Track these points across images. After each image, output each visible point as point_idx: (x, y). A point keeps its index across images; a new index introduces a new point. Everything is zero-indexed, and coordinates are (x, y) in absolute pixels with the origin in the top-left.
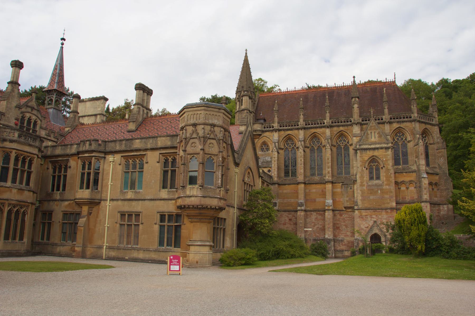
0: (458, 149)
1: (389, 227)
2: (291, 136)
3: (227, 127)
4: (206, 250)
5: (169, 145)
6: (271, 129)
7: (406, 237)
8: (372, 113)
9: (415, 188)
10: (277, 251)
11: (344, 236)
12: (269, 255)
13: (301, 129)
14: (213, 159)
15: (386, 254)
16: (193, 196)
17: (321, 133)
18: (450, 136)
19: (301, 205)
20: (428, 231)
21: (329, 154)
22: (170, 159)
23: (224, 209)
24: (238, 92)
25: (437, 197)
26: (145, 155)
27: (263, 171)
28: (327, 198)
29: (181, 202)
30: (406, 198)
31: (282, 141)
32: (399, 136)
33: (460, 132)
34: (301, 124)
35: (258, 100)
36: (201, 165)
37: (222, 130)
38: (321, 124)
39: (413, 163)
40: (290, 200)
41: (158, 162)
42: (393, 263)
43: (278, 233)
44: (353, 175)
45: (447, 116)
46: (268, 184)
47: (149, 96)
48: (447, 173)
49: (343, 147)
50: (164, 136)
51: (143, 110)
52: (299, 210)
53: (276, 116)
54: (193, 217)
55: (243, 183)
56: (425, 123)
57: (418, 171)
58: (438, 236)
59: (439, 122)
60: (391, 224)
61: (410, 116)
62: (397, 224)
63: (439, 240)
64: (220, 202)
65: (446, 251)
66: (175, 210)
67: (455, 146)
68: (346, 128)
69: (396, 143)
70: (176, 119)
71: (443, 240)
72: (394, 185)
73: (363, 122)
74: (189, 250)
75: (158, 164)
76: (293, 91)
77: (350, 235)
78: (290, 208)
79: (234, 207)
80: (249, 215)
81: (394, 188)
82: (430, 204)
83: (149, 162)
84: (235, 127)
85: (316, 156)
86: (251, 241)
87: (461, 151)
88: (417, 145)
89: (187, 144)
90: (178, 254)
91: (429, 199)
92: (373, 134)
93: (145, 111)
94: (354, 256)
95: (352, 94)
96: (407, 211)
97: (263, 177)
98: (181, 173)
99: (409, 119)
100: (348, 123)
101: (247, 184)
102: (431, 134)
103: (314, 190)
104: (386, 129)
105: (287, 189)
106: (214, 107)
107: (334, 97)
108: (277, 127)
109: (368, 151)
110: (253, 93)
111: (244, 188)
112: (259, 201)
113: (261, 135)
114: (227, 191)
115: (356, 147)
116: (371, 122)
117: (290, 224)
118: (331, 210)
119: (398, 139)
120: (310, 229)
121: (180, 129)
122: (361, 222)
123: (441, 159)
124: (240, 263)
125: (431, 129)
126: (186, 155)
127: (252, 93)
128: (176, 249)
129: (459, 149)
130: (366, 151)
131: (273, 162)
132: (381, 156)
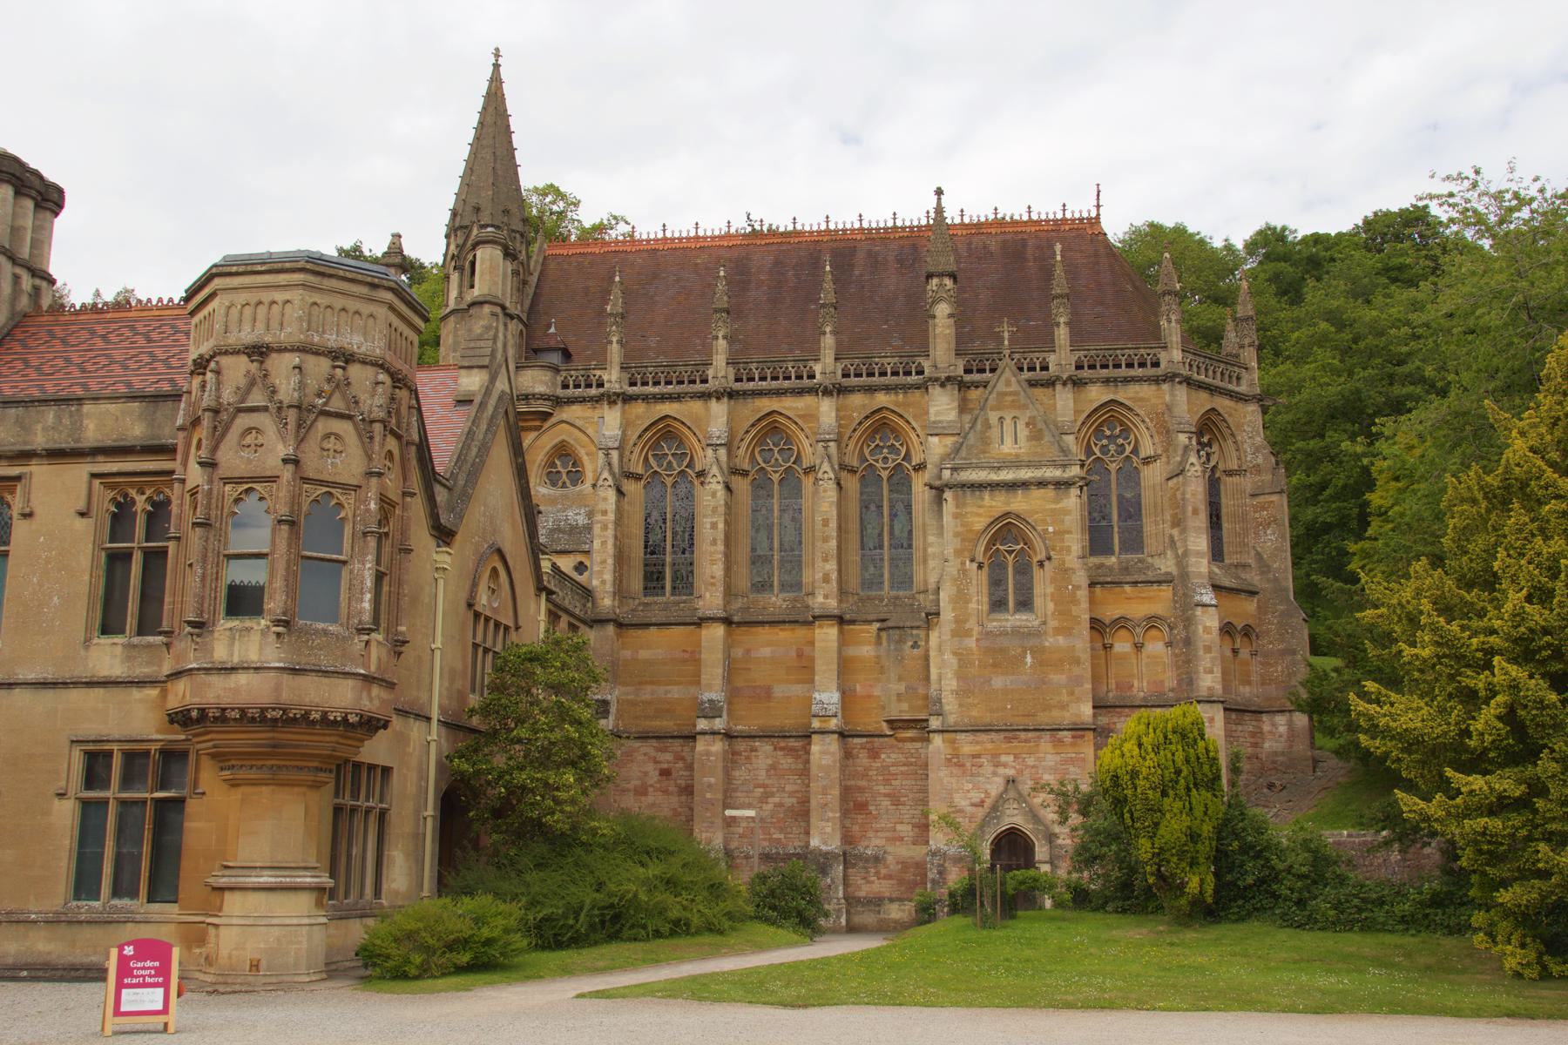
0: (1320, 498)
1: (1068, 804)
4: (299, 908)
5: (135, 438)
6: (593, 391)
7: (1142, 841)
8: (1006, 342)
9: (1169, 644)
10: (612, 906)
11: (888, 839)
12: (578, 926)
13: (718, 395)
14: (340, 505)
15: (1059, 912)
16: (244, 668)
17: (799, 416)
19: (712, 711)
20: (1227, 819)
22: (141, 503)
23: (385, 726)
24: (457, 228)
25: (1249, 683)
26: (18, 478)
27: (555, 568)
28: (817, 683)
29: (188, 694)
34: (720, 375)
35: (539, 269)
36: (285, 527)
37: (382, 377)
40: (667, 692)
41: (82, 514)
42: (1092, 950)
43: (618, 828)
44: (925, 591)
45: (1281, 368)
47: (48, 214)
49: (885, 474)
50: (114, 398)
51: (16, 278)
52: (703, 733)
53: (615, 339)
54: (240, 763)
55: (471, 616)
57: (1179, 581)
58: (1265, 837)
60: (1077, 788)
61: (1154, 359)
62: (1106, 791)
64: (365, 694)
65: (1295, 895)
66: (158, 732)
67: (1311, 485)
69: (1095, 465)
71: (1281, 853)
72: (1086, 632)
73: (968, 378)
75: (81, 524)
77: (911, 834)
78: (665, 723)
79: (429, 719)
80: (491, 753)
81: (1089, 645)
83: (38, 510)
85: (776, 507)
86: (499, 866)
87: (1334, 506)
88: (1177, 475)
89: (223, 435)
90: (163, 933)
91: (1220, 692)
92: (1008, 422)
93: (27, 282)
94: (929, 922)
95: (928, 259)
96: (1147, 734)
97: (552, 593)
98: (191, 565)
99: (1150, 371)
100: (909, 378)
101: (487, 619)
102: (1233, 435)
103: (766, 652)
104: (1058, 407)
105: (656, 646)
106: (349, 275)
107: (857, 273)
108: (617, 386)
109: (987, 495)
110: (522, 235)
112: (534, 691)
114: (398, 645)
115: (940, 478)
116: (1003, 378)
117: (666, 792)
118: (833, 732)
119: (1104, 450)
120: (751, 813)
121: (190, 366)
122: (953, 780)
123: (1269, 532)
124: (449, 964)
125: (1230, 415)
126: (217, 485)
127: (518, 236)
128: (156, 907)
129: (1326, 501)
131: (597, 529)
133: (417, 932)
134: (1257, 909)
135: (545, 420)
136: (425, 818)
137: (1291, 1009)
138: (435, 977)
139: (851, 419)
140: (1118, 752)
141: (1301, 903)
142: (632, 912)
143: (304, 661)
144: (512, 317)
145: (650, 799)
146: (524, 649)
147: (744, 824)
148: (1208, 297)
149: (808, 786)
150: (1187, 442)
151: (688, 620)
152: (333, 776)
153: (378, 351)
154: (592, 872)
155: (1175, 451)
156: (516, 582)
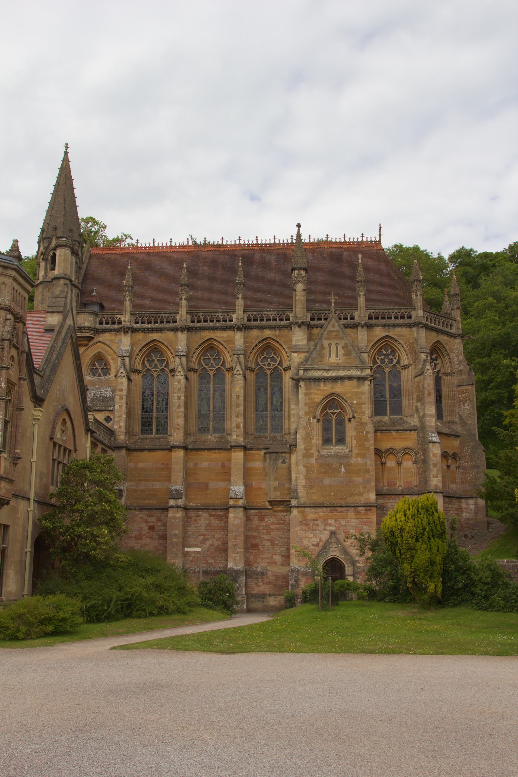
1: (365, 545)
2: (160, 344)
3: (21, 312)
6: (116, 326)
7: (405, 565)
8: (333, 305)
9: (415, 462)
10: (127, 599)
11: (268, 563)
12: (110, 610)
13: (182, 330)
15: (361, 602)
17: (225, 341)
18: (475, 362)
19: (177, 495)
21: (241, 387)
23: (8, 503)
24: (44, 238)
25: (455, 483)
28: (232, 481)
30: (396, 484)
31: (138, 354)
32: (386, 355)
33: (494, 354)
34: (183, 319)
35: (87, 261)
37: (9, 316)
38: (225, 321)
42: (380, 622)
43: (130, 558)
44: (289, 434)
46: (106, 448)
48: (475, 435)
49: (269, 372)
52: (172, 507)
53: (128, 299)
55: (51, 444)
58: (468, 563)
59: (462, 330)
60: (369, 537)
62: (387, 539)
63: (469, 572)
65: (483, 593)
67: (484, 380)
68: (278, 332)
69: (378, 370)
72: (372, 456)
73: (312, 323)
76: (166, 247)
77: (280, 560)
78: (152, 501)
79: (29, 499)
80: (62, 517)
81: (374, 463)
82: (444, 496)
85: (211, 389)
87: (496, 391)
88: (420, 375)
92: (333, 346)
94: (291, 607)
95: (293, 261)
96: (409, 509)
99: (406, 321)
100: (282, 322)
101: (60, 446)
102: (448, 355)
103: (206, 464)
104: (359, 338)
107: (255, 267)
108: (129, 324)
109: (322, 384)
110: (79, 243)
111: (53, 456)
113: (93, 338)
114: (15, 460)
115: (298, 374)
116: (331, 323)
117: (152, 538)
119: (382, 361)
120: (199, 550)
123: (466, 405)
125: (447, 344)
127: (77, 243)
129: (491, 389)
130: (317, 383)
131: (117, 399)
132: (347, 395)
133: (24, 614)
134: (464, 601)
135: (90, 341)
136: (26, 552)
137: (486, 653)
138: (34, 639)
139: (251, 343)
140: (394, 519)
141: (486, 597)
142: (138, 603)
144: (75, 286)
145: (143, 542)
146: (81, 462)
147: (193, 555)
148: (431, 284)
149: (227, 535)
150: (425, 357)
151: (165, 447)
153: (7, 302)
154: (116, 581)
155: (419, 362)
156: (75, 426)
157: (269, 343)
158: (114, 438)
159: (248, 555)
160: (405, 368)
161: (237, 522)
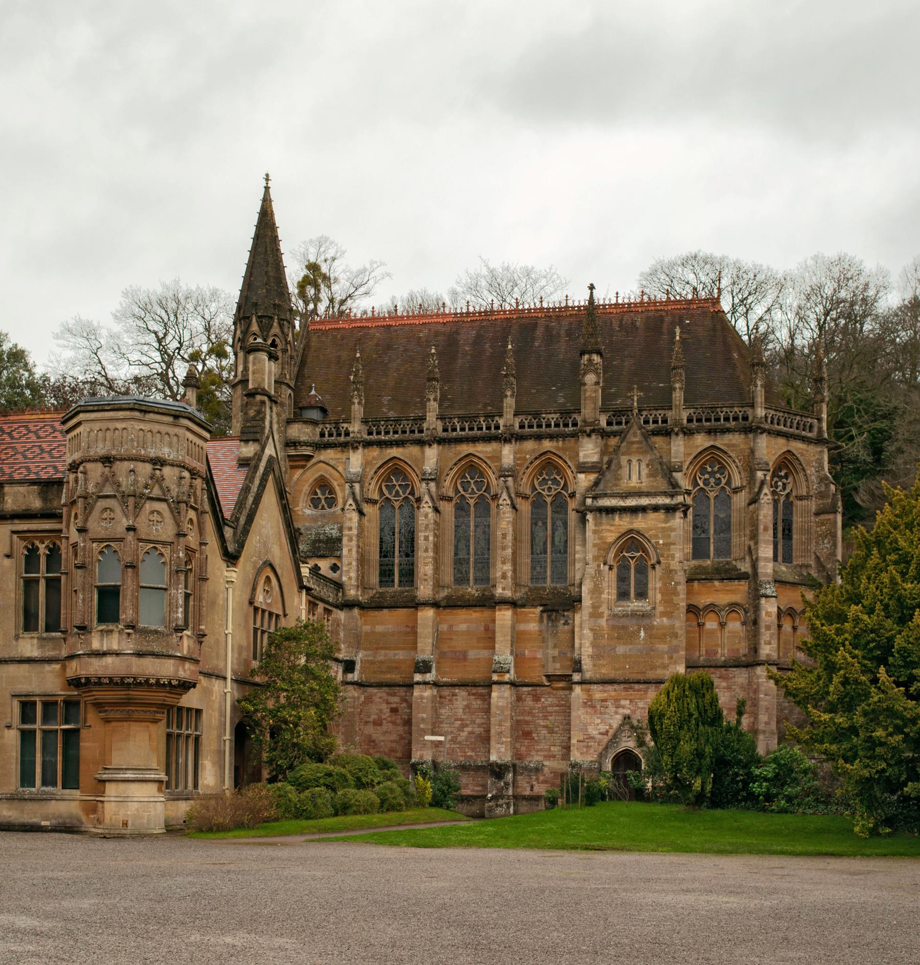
6: (342, 439)
9: (744, 623)
11: (545, 756)
17: (489, 458)
19: (424, 667)
21: (508, 522)
22: (42, 549)
23: (194, 686)
32: (712, 474)
36: (130, 570)
39: (742, 554)
40: (395, 655)
41: (8, 556)
49: (549, 500)
52: (418, 683)
55: (252, 609)
56: (787, 436)
57: (752, 577)
64: (181, 668)
66: (62, 690)
68: (561, 443)
70: (52, 426)
72: (683, 616)
73: (609, 429)
74: (102, 793)
75: (7, 562)
78: (394, 676)
79: (225, 678)
84: (229, 443)
85: (472, 524)
89: (90, 512)
92: (635, 463)
98: (75, 591)
101: (263, 611)
102: (804, 470)
103: (463, 627)
104: (672, 451)
111: (255, 624)
113: (312, 456)
114: (200, 637)
117: (394, 723)
118: (507, 683)
119: (706, 482)
122: (588, 717)
123: (826, 541)
125: (802, 455)
128: (67, 791)
131: (345, 540)
139: (525, 459)
143: (145, 648)
152: (165, 715)
156: (283, 584)
157: (549, 458)
158: (343, 593)
159: (518, 745)
160: (736, 492)
161: (501, 703)
